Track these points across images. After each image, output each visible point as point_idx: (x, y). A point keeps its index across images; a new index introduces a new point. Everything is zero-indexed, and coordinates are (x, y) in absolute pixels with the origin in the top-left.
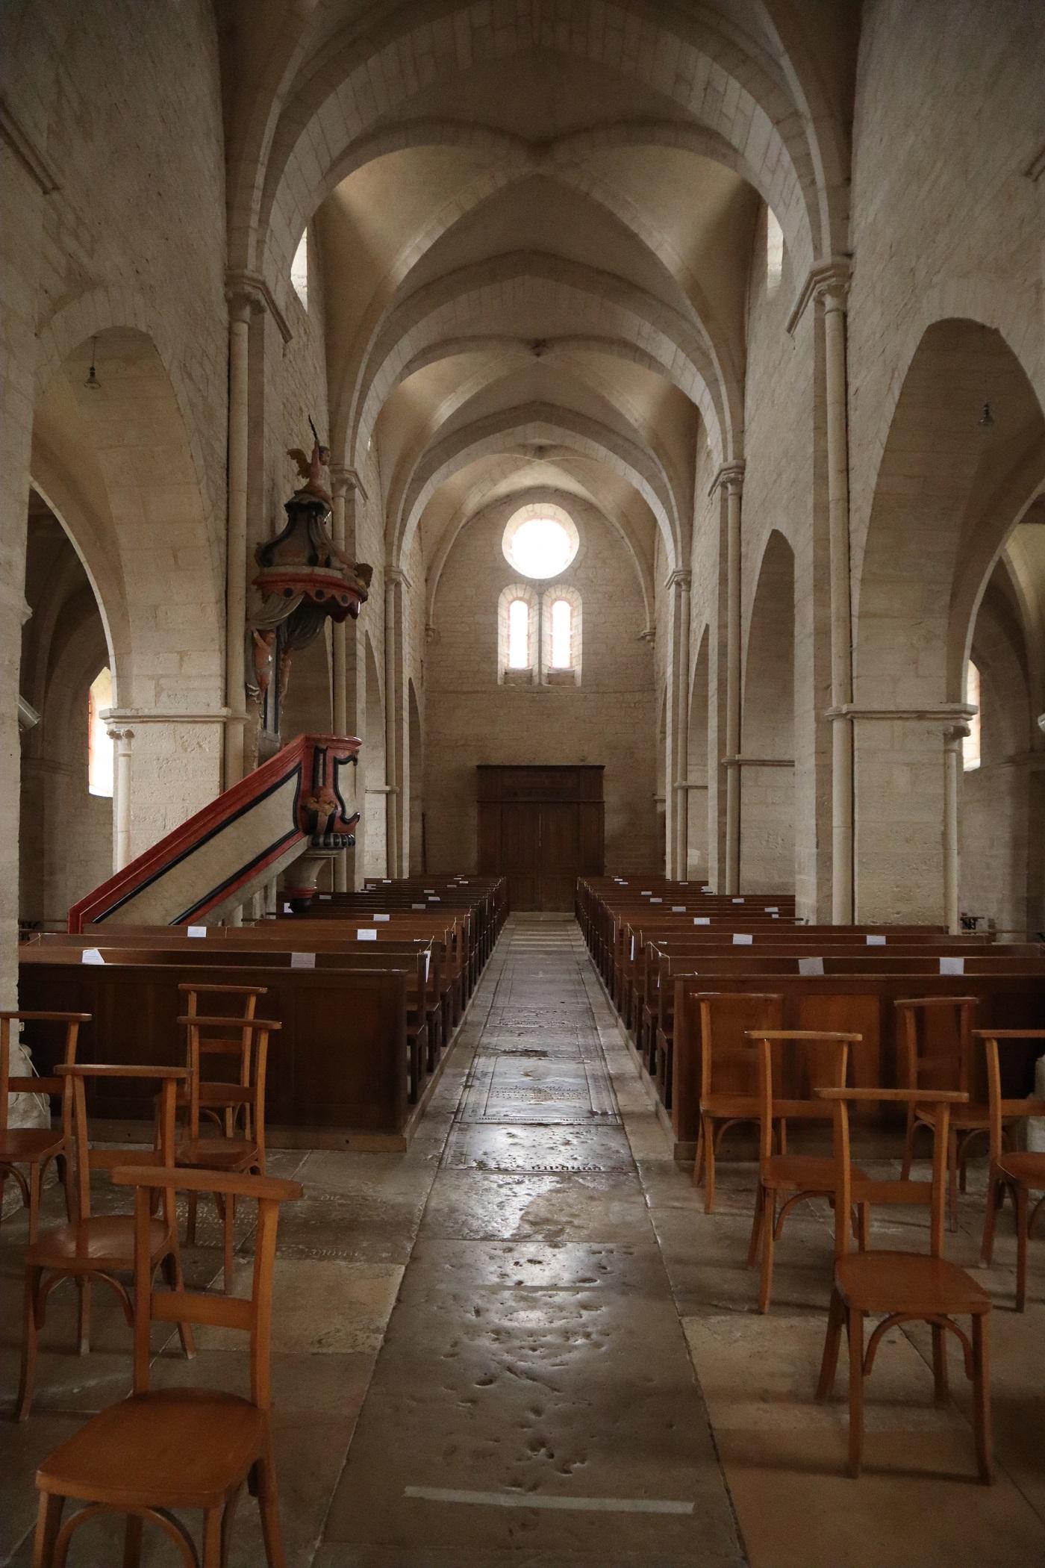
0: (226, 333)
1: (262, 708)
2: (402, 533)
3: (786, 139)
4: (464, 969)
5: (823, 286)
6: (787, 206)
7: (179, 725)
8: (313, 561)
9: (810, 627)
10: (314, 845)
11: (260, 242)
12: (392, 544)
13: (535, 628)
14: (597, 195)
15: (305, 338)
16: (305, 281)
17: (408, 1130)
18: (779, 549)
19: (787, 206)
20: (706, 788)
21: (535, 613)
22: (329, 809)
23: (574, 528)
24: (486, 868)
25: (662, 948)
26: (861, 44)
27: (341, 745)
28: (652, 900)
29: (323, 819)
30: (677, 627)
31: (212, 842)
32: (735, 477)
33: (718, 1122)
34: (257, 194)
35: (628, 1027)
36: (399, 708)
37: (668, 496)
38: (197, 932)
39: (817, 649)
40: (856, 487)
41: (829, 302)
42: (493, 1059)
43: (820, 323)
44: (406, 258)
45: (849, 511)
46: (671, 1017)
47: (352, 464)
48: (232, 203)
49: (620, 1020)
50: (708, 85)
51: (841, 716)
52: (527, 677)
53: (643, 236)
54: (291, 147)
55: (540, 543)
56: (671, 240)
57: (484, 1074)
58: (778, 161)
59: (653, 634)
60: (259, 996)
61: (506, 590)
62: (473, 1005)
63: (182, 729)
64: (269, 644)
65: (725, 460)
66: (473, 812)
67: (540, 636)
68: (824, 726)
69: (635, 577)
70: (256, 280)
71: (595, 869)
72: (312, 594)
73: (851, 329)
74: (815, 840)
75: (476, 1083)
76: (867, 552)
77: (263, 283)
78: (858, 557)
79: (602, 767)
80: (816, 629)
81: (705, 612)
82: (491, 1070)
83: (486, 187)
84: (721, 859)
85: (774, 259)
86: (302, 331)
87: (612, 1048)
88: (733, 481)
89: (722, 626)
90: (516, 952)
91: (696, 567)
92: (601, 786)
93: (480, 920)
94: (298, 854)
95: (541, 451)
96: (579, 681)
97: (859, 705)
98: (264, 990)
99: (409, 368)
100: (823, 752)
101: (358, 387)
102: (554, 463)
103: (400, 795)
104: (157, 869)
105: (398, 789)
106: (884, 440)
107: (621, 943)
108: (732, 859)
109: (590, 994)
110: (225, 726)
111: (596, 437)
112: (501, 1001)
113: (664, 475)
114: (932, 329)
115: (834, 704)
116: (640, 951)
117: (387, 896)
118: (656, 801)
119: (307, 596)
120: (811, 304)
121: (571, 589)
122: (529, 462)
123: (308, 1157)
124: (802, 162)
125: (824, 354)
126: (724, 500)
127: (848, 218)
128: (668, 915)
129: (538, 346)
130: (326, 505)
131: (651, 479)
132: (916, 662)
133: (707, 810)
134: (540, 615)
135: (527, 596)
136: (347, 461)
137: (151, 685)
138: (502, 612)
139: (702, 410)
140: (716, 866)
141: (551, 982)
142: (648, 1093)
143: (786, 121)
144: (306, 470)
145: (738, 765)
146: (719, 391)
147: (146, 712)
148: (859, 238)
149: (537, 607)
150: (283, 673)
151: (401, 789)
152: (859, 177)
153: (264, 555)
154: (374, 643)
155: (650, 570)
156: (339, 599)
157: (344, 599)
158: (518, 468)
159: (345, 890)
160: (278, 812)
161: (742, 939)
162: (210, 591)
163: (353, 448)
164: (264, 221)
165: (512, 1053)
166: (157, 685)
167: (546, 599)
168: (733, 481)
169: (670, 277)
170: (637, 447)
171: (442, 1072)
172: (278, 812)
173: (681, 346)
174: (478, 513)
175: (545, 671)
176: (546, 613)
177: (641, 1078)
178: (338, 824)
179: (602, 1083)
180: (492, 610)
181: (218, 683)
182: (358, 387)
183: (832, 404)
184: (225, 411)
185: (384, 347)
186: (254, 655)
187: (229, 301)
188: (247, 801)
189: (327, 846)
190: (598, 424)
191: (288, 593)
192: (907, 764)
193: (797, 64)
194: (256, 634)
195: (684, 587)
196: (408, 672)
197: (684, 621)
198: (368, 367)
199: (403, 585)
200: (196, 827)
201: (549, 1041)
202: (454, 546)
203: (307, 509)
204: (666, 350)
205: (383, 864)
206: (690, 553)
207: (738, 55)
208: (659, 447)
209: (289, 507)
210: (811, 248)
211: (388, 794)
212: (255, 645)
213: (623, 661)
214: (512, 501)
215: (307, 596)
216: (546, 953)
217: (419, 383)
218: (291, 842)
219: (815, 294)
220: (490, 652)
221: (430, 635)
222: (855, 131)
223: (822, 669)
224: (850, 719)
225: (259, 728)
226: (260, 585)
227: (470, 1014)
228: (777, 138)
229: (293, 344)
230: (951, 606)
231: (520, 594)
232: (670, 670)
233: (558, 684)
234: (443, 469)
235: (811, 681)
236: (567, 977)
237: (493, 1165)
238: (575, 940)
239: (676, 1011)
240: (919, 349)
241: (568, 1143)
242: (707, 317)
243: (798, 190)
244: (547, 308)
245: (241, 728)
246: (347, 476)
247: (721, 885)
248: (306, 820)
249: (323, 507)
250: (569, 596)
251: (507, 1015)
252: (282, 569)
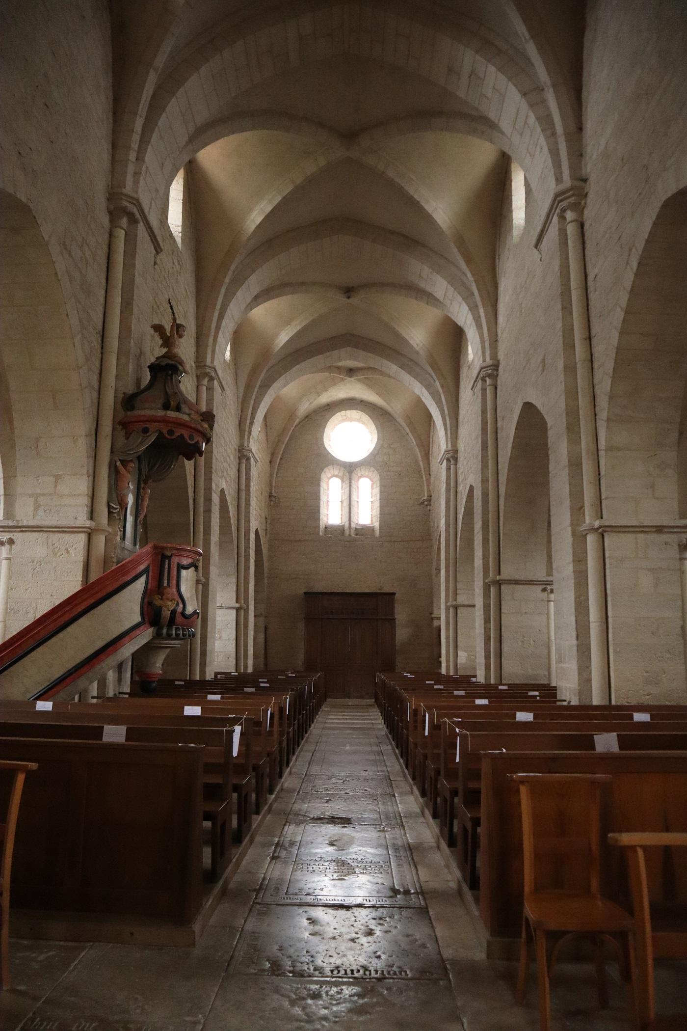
0: (107, 236)
1: (122, 523)
2: (252, 423)
3: (532, 105)
4: (280, 743)
5: (564, 204)
6: (532, 156)
7: (51, 535)
8: (166, 407)
9: (564, 460)
10: (158, 635)
11: (137, 174)
12: (245, 431)
13: (346, 496)
14: (390, 173)
15: (178, 267)
16: (180, 229)
17: (200, 918)
18: (531, 417)
19: (532, 156)
20: (474, 606)
21: (346, 486)
22: (171, 605)
23: (373, 427)
24: (310, 666)
25: (458, 724)
26: (587, 33)
27: (185, 553)
28: (436, 687)
29: (166, 614)
30: (448, 490)
31: (69, 629)
32: (491, 373)
33: (553, 936)
34: (136, 138)
35: (423, 794)
36: (247, 548)
37: (440, 399)
38: (44, 706)
39: (571, 477)
40: (599, 349)
41: (570, 215)
42: (302, 826)
43: (563, 233)
44: (255, 218)
45: (592, 368)
46: (478, 792)
47: (212, 361)
48: (117, 142)
49: (415, 789)
50: (472, 73)
51: (594, 530)
52: (340, 530)
53: (423, 203)
54: (163, 109)
55: (350, 437)
56: (444, 208)
57: (292, 844)
58: (526, 122)
59: (430, 500)
60: (29, 774)
61: (326, 470)
62: (290, 773)
63: (55, 537)
64: (129, 472)
65: (484, 361)
66: (301, 626)
67: (351, 502)
68: (579, 539)
69: (417, 462)
70: (132, 198)
71: (389, 667)
72: (165, 431)
73: (587, 234)
74: (574, 634)
75: (283, 854)
76: (612, 397)
77: (138, 200)
78: (603, 402)
79: (394, 594)
80: (569, 461)
81: (470, 474)
82: (298, 839)
83: (310, 167)
84: (487, 657)
85: (519, 214)
86: (176, 262)
87: (409, 815)
88: (489, 376)
89: (485, 481)
90: (330, 729)
91: (461, 446)
92: (393, 608)
93: (298, 702)
94: (143, 642)
95: (351, 372)
96: (377, 533)
97: (609, 519)
98: (33, 766)
99: (258, 299)
100: (580, 560)
101: (218, 307)
102: (359, 380)
103: (246, 611)
104: (21, 652)
105: (245, 606)
106: (624, 305)
107: (415, 721)
108: (495, 655)
109: (388, 763)
110: (90, 536)
111: (388, 357)
112: (315, 769)
113: (437, 383)
114: (668, 204)
115: (587, 521)
116: (435, 727)
117: (228, 684)
118: (432, 619)
119: (161, 434)
120: (555, 219)
121: (372, 469)
122: (343, 380)
123: (88, 954)
124: (546, 122)
125: (568, 254)
126: (484, 390)
127: (581, 155)
128: (451, 697)
129: (349, 291)
130: (180, 368)
131: (428, 387)
132: (653, 486)
133: (474, 625)
134: (350, 486)
135: (341, 474)
136: (209, 360)
137: (31, 501)
138: (323, 485)
139: (466, 329)
140: (483, 661)
141: (354, 753)
142: (447, 866)
143: (532, 94)
144: (167, 342)
145: (499, 584)
146: (479, 313)
147: (25, 523)
148: (591, 167)
149: (347, 482)
150: (143, 500)
151: (248, 606)
152: (590, 125)
153: (129, 402)
154: (229, 499)
155: (427, 455)
156: (187, 437)
157: (191, 438)
158: (335, 384)
159: (198, 678)
160: (128, 605)
161: (524, 716)
162: (82, 426)
163: (213, 352)
164: (140, 158)
165: (319, 820)
166: (36, 501)
167: (354, 476)
168: (489, 376)
169: (443, 232)
170: (416, 363)
171: (252, 841)
172: (128, 605)
173: (451, 283)
174: (307, 417)
175: (353, 526)
176: (354, 486)
177: (438, 847)
178: (179, 619)
179: (402, 853)
180: (317, 483)
181: (85, 501)
182: (218, 307)
183: (575, 293)
184: (103, 292)
185: (238, 281)
186: (116, 480)
187: (110, 213)
188: (100, 596)
189: (169, 636)
190: (392, 349)
191: (146, 431)
192: (649, 570)
193: (540, 47)
194: (118, 463)
195: (452, 462)
196: (254, 524)
197: (453, 487)
198: (225, 295)
199: (252, 460)
200: (55, 617)
201: (353, 808)
202: (291, 439)
203: (166, 369)
204: (440, 287)
205: (233, 662)
206: (456, 438)
207: (493, 47)
208: (434, 365)
209: (152, 368)
210: (554, 179)
211: (238, 610)
212: (117, 471)
213: (408, 522)
214: (331, 408)
215: (161, 434)
216: (353, 729)
217: (263, 314)
218: (138, 632)
219: (558, 210)
220: (314, 512)
221: (272, 500)
222: (584, 94)
223: (577, 495)
224: (602, 532)
225: (118, 539)
226: (124, 425)
227: (288, 781)
228: (524, 105)
229: (162, 256)
230: (679, 442)
231: (336, 473)
232: (443, 522)
233: (362, 535)
234: (282, 380)
235: (567, 502)
236: (369, 749)
237: (287, 964)
238: (376, 720)
239: (484, 786)
240: (655, 224)
241: (370, 933)
242: (468, 260)
243: (542, 141)
244: (352, 250)
245: (102, 538)
246: (208, 370)
247: (487, 676)
248: (151, 613)
249: (177, 369)
250: (370, 474)
251: (319, 782)
252: (142, 412)
